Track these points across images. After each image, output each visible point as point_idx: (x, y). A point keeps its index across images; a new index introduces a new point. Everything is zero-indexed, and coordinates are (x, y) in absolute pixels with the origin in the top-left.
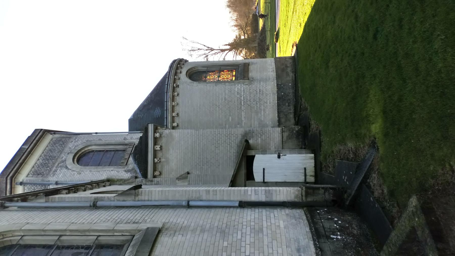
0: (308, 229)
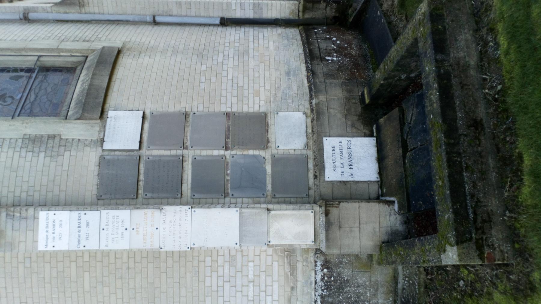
0: (301, 51)
